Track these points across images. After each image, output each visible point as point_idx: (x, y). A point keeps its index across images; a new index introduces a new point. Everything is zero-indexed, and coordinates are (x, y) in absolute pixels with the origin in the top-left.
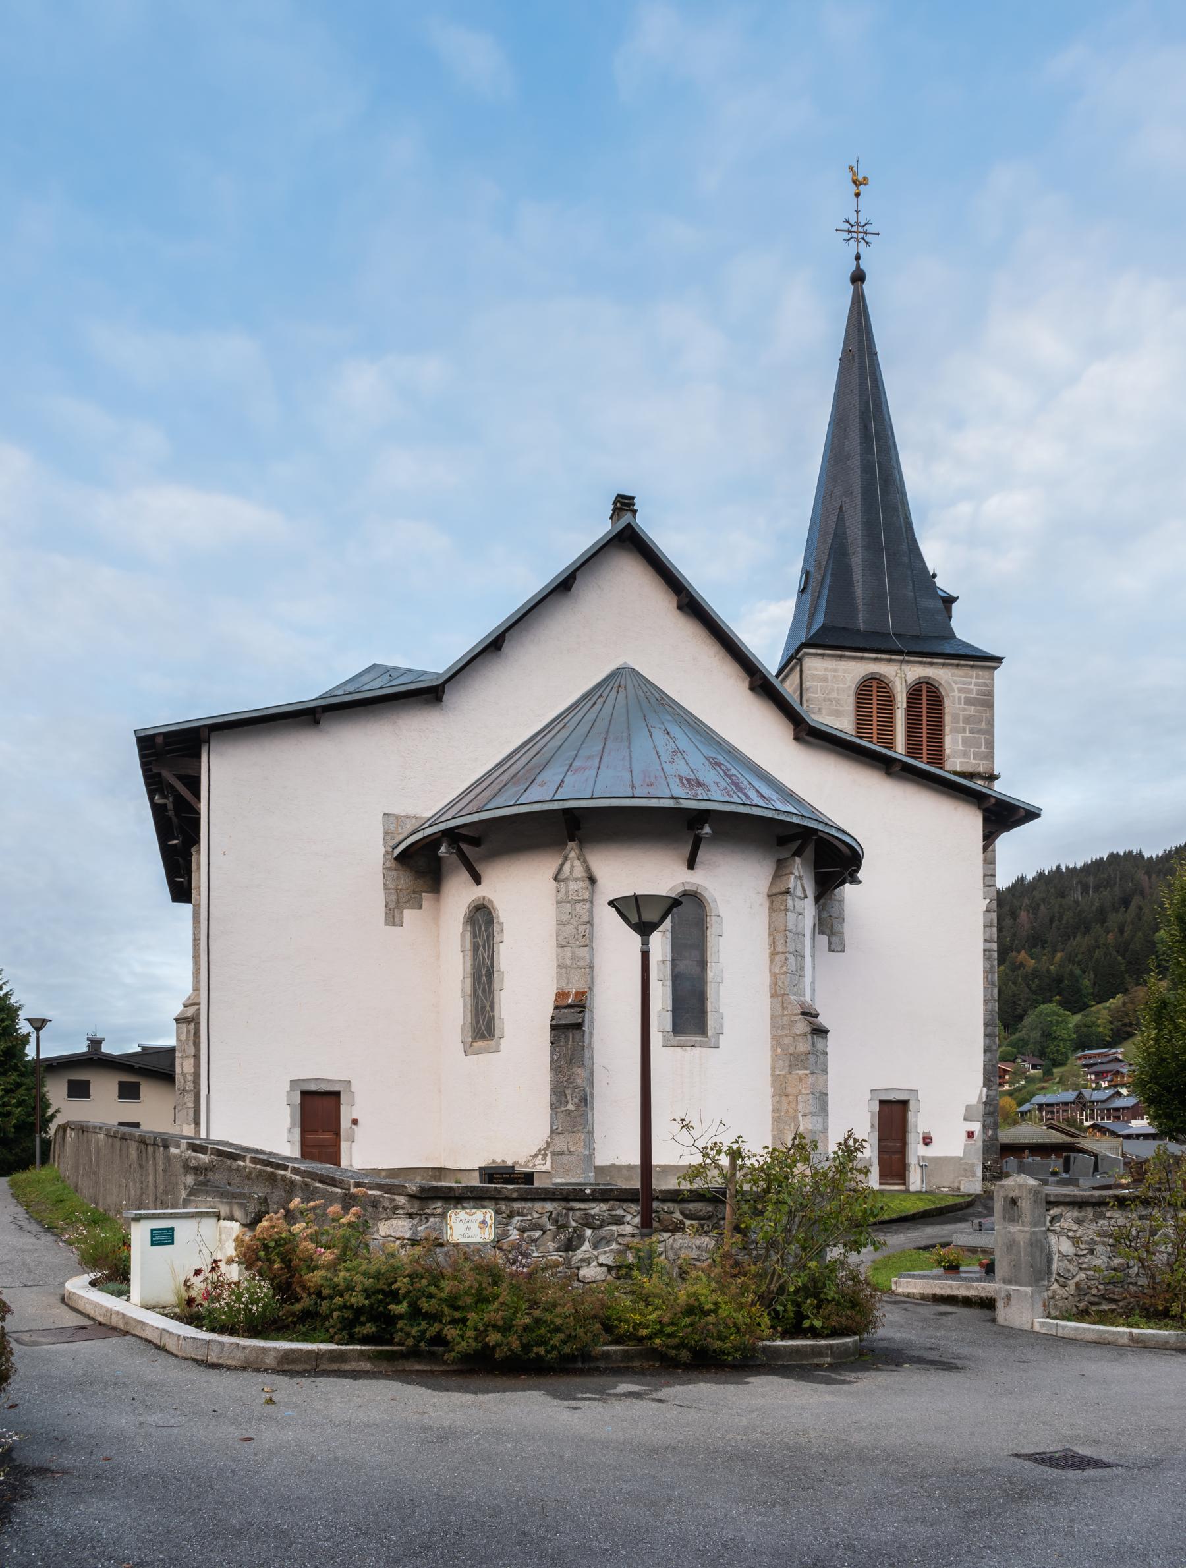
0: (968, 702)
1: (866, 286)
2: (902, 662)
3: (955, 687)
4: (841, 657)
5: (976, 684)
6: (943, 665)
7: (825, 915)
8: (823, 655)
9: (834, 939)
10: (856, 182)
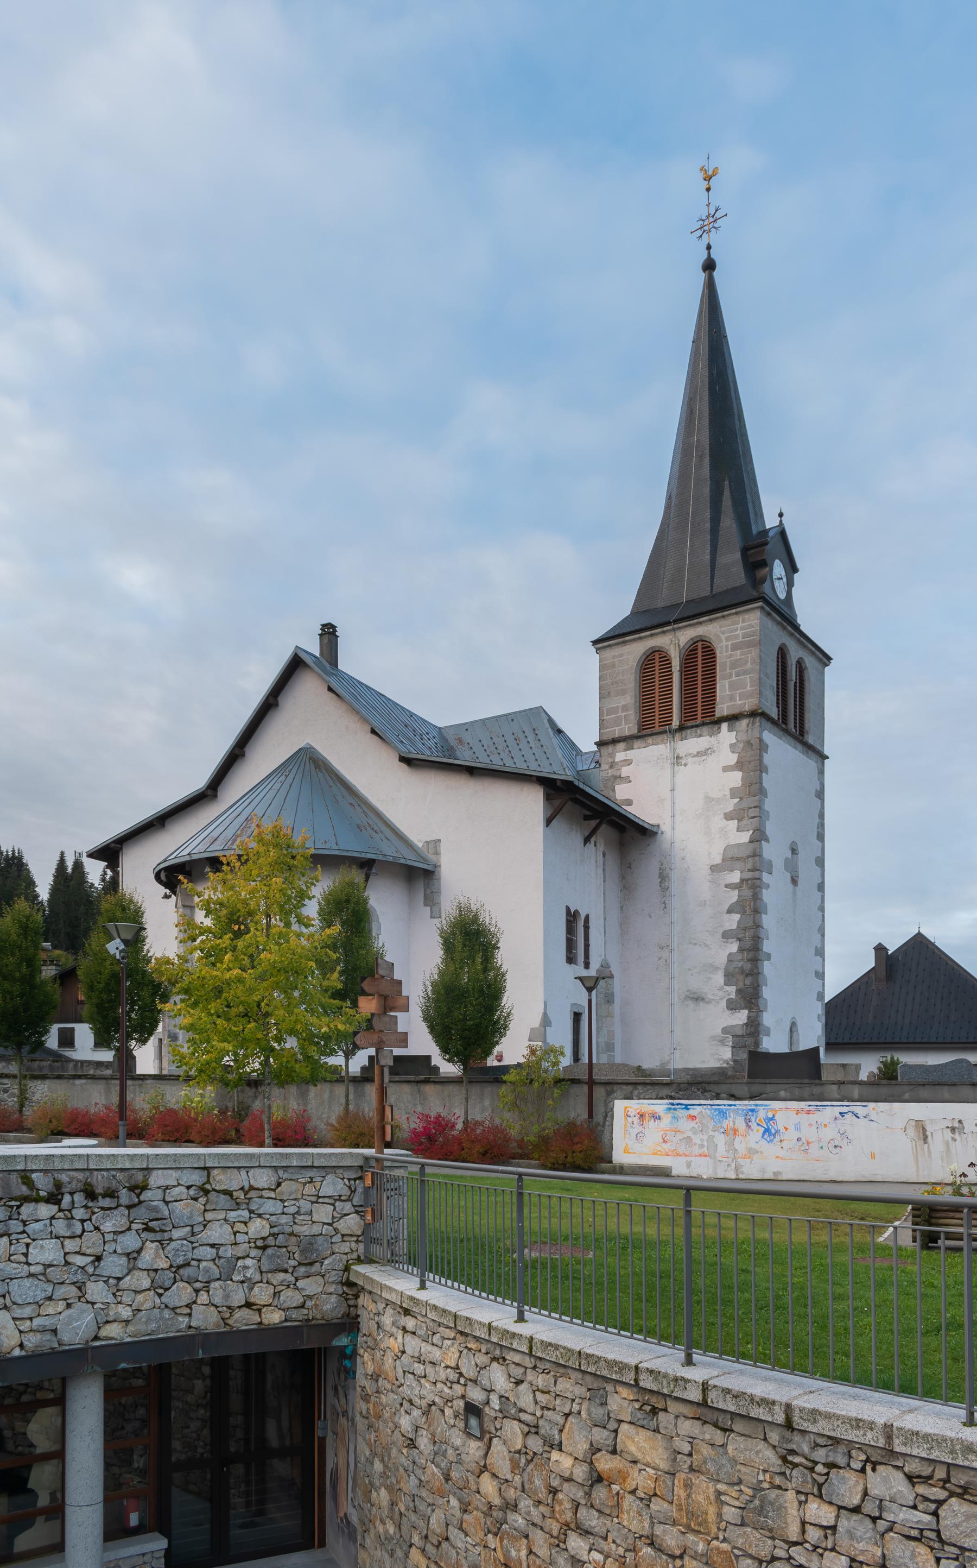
0: (735, 647)
1: (716, 274)
2: (674, 630)
3: (723, 637)
4: (624, 642)
5: (742, 629)
6: (711, 620)
7: (428, 892)
8: (609, 646)
9: (435, 908)
10: (708, 178)
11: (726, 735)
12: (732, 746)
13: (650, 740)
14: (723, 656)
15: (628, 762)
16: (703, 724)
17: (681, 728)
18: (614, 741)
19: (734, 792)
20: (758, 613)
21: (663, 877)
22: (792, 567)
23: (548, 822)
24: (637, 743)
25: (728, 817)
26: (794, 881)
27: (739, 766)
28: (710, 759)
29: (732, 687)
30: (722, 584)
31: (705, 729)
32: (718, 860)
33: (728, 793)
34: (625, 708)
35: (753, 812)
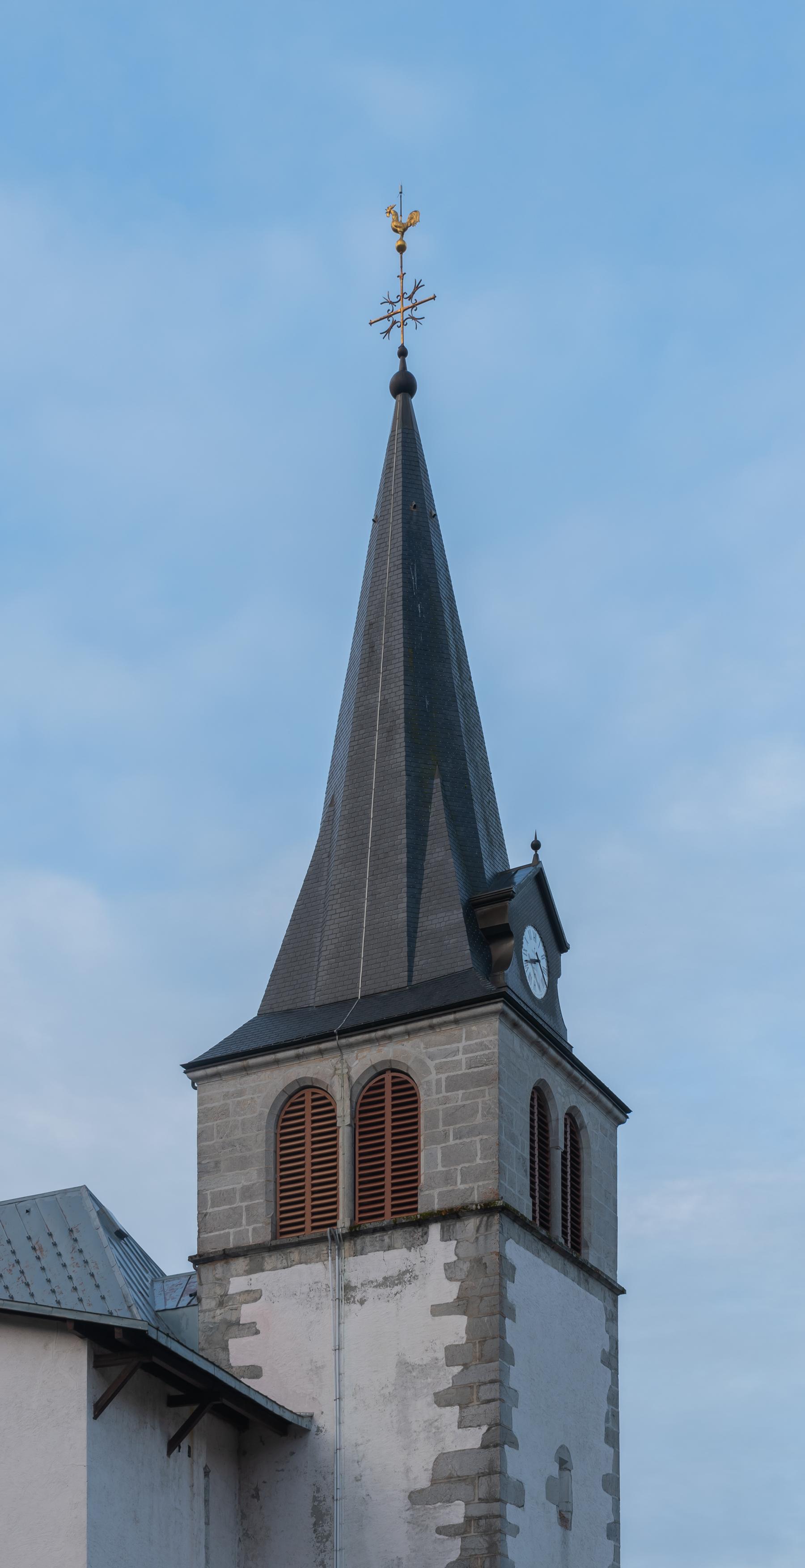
0: (453, 1084)
3: (431, 1064)
5: (466, 1051)
6: (408, 1033)
8: (218, 1075)
10: (401, 229)
11: (438, 1248)
12: (448, 1267)
13: (295, 1254)
14: (431, 1101)
15: (253, 1296)
16: (396, 1226)
17: (354, 1233)
18: (227, 1256)
19: (452, 1354)
20: (495, 1023)
21: (321, 1514)
22: (557, 942)
23: (98, 1409)
24: (270, 1260)
25: (442, 1400)
26: (565, 1521)
27: (462, 1305)
28: (409, 1290)
29: (449, 1157)
30: (428, 967)
31: (398, 1235)
32: (423, 1481)
33: (441, 1355)
34: (247, 1193)
35: (487, 1392)
